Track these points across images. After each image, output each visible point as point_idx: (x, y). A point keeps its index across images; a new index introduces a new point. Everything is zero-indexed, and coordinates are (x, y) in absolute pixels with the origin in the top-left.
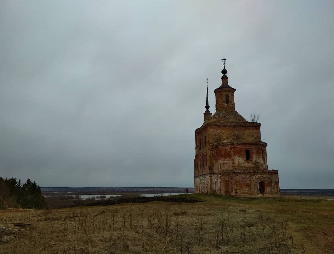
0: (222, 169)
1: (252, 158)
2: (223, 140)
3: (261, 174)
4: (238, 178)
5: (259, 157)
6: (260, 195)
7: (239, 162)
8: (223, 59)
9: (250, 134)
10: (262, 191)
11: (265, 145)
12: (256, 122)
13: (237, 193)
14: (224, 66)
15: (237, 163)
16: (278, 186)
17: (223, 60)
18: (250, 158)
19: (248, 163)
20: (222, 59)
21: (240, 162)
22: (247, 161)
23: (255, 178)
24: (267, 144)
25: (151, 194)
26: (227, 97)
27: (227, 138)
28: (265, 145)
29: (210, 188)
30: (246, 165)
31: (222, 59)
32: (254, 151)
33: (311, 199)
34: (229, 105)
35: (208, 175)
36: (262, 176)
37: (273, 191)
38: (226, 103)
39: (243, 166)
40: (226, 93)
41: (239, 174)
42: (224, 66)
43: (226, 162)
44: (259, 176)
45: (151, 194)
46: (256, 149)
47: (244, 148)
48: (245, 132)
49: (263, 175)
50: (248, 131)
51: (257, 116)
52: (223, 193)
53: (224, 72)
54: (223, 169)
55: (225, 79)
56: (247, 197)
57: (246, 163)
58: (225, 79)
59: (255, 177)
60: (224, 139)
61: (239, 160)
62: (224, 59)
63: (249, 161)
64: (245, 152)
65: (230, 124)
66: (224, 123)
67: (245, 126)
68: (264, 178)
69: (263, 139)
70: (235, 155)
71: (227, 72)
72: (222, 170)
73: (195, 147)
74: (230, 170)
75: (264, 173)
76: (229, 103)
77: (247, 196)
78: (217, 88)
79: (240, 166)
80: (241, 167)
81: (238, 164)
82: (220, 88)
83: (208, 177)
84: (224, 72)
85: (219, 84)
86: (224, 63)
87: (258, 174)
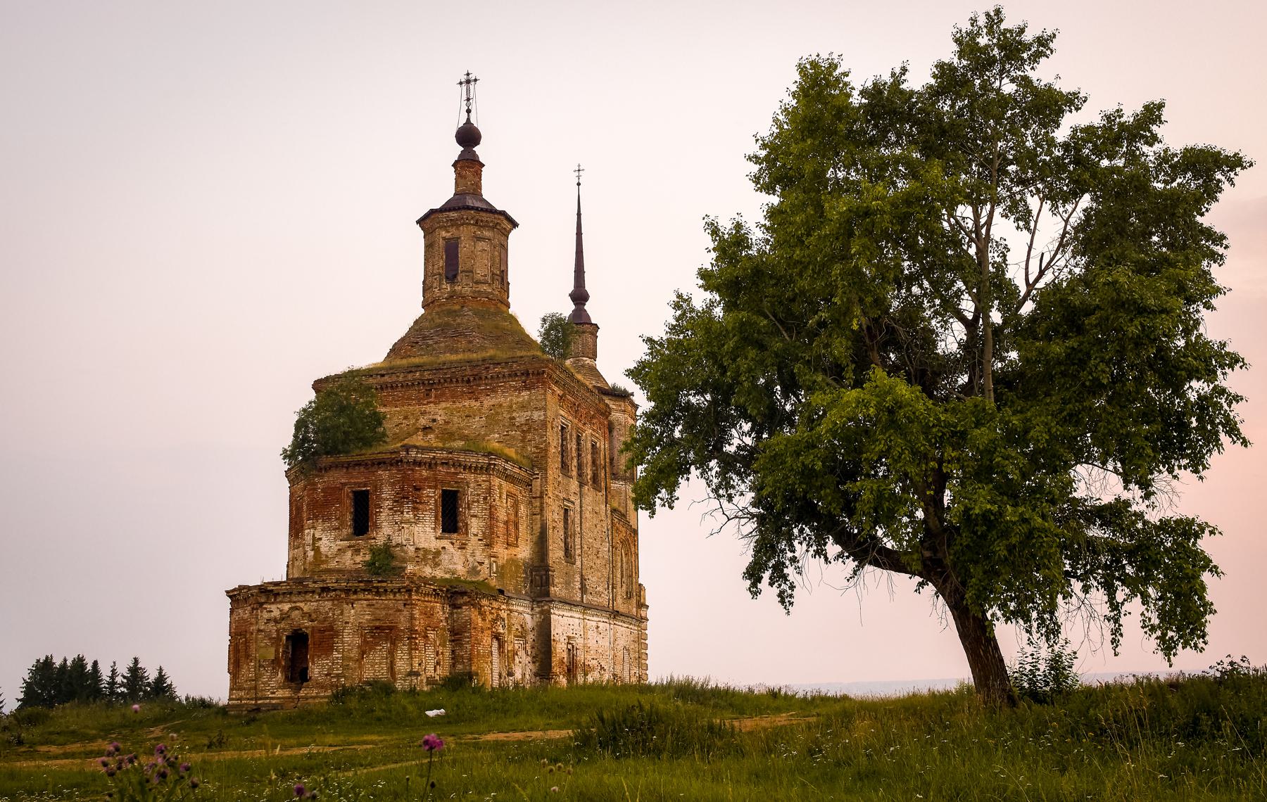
1: (377, 527)
3: (294, 599)
7: (317, 550)
8: (464, 79)
9: (497, 413)
10: (297, 675)
14: (469, 111)
17: (464, 87)
20: (461, 83)
21: (323, 549)
32: (387, 493)
33: (763, 724)
34: (458, 288)
36: (297, 608)
38: (447, 278)
39: (333, 565)
40: (448, 235)
42: (469, 111)
44: (286, 607)
46: (393, 485)
47: (344, 484)
49: (302, 605)
50: (488, 402)
53: (468, 137)
55: (468, 166)
57: (349, 553)
58: (468, 166)
59: (266, 615)
62: (468, 82)
64: (348, 502)
65: (410, 377)
66: (383, 375)
67: (477, 377)
68: (304, 614)
75: (370, 591)
79: (324, 566)
81: (315, 557)
84: (468, 137)
85: (442, 190)
87: (281, 602)
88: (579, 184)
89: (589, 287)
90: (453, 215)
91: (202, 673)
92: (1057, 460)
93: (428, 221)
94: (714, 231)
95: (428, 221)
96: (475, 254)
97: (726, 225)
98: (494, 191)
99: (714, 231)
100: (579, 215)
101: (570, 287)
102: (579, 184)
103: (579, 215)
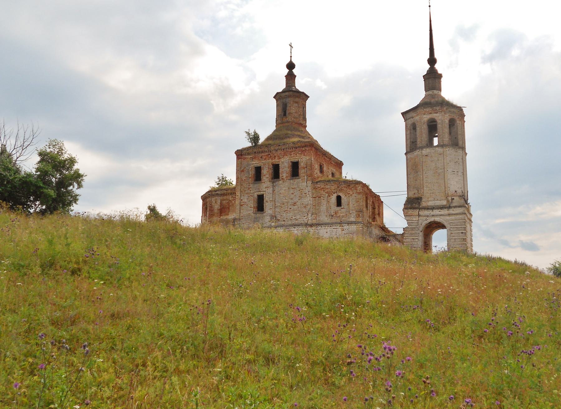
53: (291, 66)
55: (291, 77)
58: (291, 77)
84: (291, 66)
85: (282, 86)
88: (430, 6)
89: (436, 56)
90: (287, 93)
91: (191, 216)
92: (47, 205)
93: (277, 96)
94: (248, 134)
95: (277, 96)
96: (293, 109)
97: (252, 132)
98: (300, 85)
99: (248, 134)
100: (430, 21)
101: (428, 56)
102: (430, 6)
103: (430, 21)
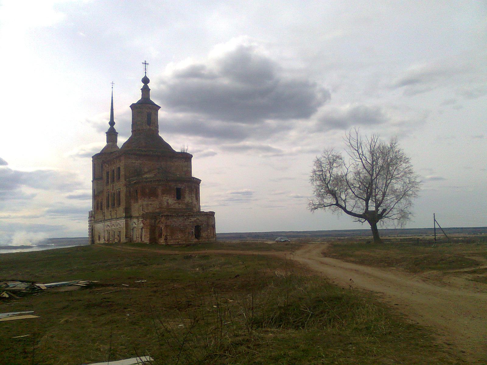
0: (145, 211)
1: (184, 197)
2: (144, 174)
4: (364, 199)
5: (192, 197)
6: (196, 240)
7: (168, 203)
8: (144, 62)
10: (198, 236)
11: (198, 182)
12: (186, 152)
13: (166, 240)
15: (166, 204)
16: (214, 230)
18: (182, 198)
19: (179, 204)
22: (178, 201)
23: (190, 222)
24: (200, 181)
25: (27, 252)
26: (149, 116)
27: (149, 172)
28: (198, 182)
29: (126, 236)
30: (177, 206)
31: (143, 63)
35: (123, 220)
37: (209, 236)
39: (172, 207)
41: (170, 218)
42: (146, 73)
43: (150, 203)
45: (27, 251)
48: (172, 164)
51: (312, 195)
52: (146, 240)
54: (146, 211)
56: (180, 244)
58: (146, 90)
60: (146, 173)
61: (168, 200)
63: (180, 201)
69: (195, 174)
70: (163, 194)
71: (149, 82)
72: (145, 213)
73: (92, 180)
74: (157, 213)
76: (151, 125)
77: (180, 243)
78: (135, 102)
80: (171, 208)
82: (139, 102)
83: (122, 222)
85: (137, 97)
86: (146, 69)
